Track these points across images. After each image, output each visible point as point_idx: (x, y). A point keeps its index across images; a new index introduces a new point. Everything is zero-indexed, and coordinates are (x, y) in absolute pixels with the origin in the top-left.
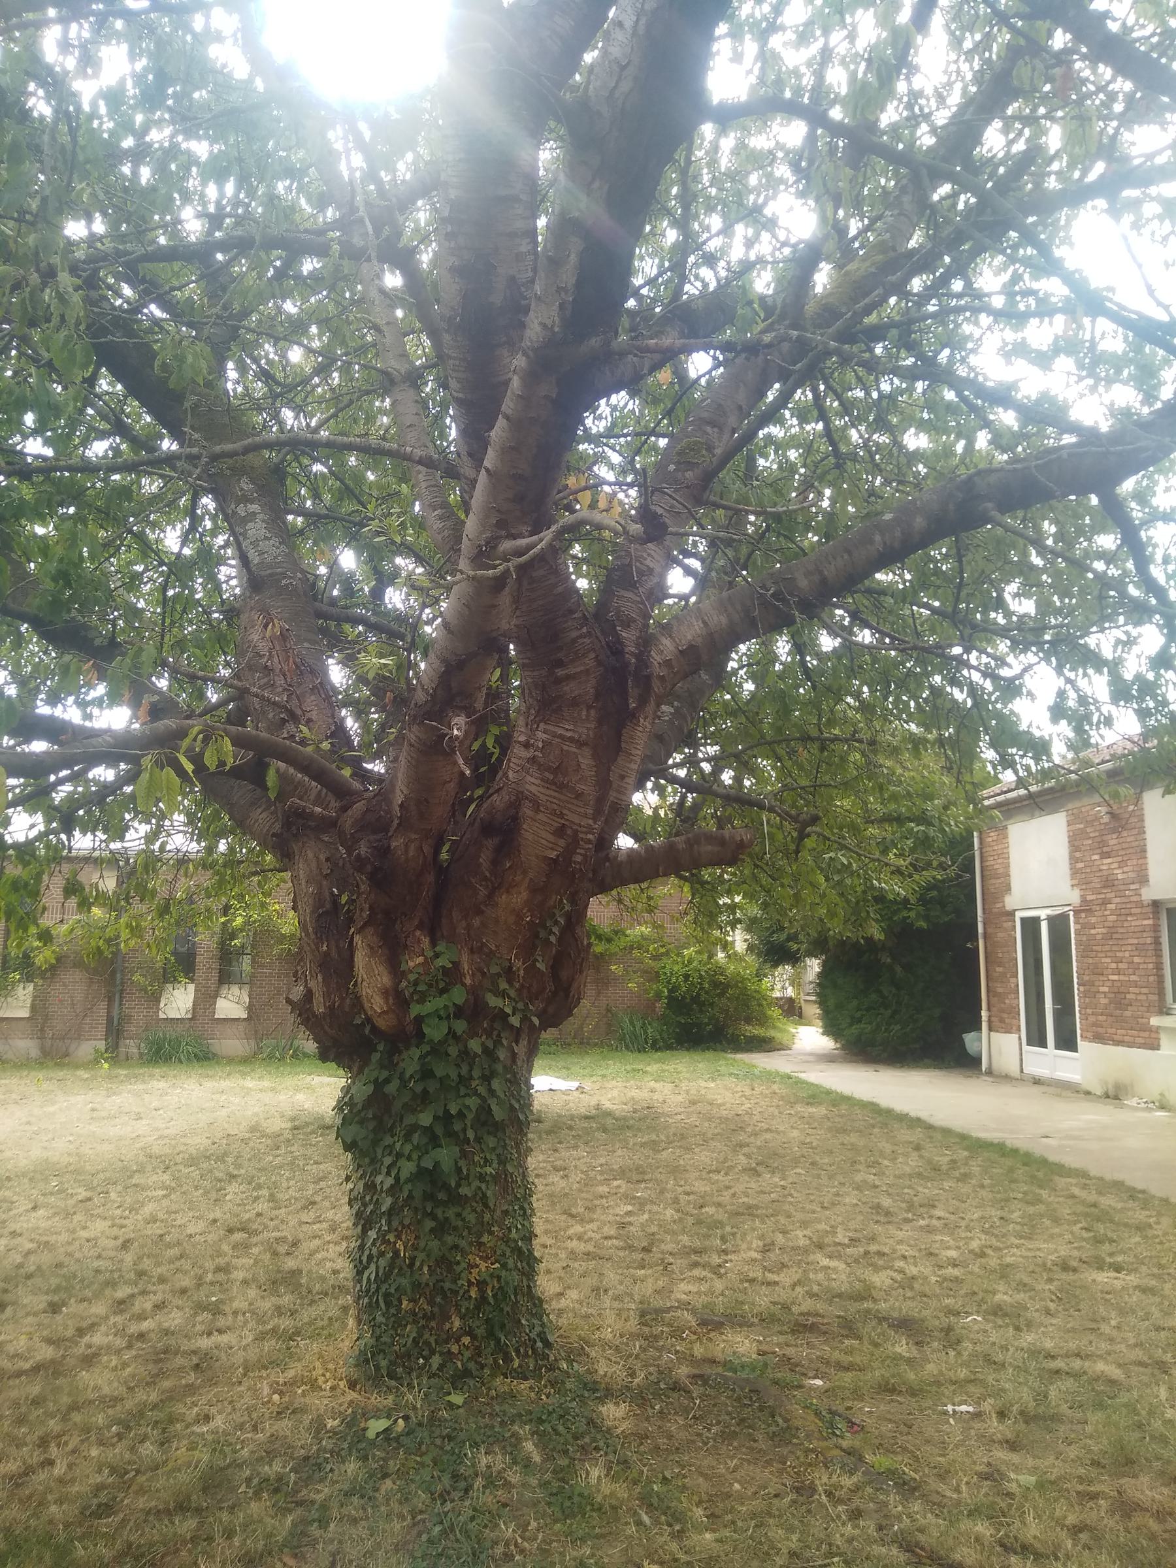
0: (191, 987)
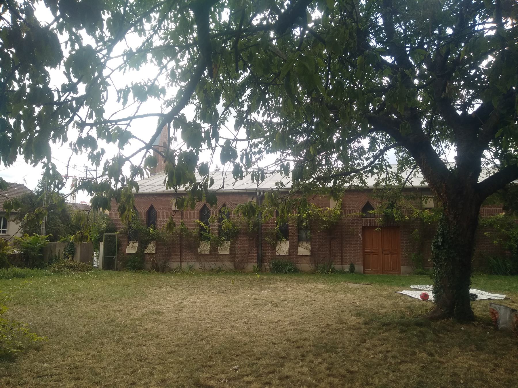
0: (288, 243)
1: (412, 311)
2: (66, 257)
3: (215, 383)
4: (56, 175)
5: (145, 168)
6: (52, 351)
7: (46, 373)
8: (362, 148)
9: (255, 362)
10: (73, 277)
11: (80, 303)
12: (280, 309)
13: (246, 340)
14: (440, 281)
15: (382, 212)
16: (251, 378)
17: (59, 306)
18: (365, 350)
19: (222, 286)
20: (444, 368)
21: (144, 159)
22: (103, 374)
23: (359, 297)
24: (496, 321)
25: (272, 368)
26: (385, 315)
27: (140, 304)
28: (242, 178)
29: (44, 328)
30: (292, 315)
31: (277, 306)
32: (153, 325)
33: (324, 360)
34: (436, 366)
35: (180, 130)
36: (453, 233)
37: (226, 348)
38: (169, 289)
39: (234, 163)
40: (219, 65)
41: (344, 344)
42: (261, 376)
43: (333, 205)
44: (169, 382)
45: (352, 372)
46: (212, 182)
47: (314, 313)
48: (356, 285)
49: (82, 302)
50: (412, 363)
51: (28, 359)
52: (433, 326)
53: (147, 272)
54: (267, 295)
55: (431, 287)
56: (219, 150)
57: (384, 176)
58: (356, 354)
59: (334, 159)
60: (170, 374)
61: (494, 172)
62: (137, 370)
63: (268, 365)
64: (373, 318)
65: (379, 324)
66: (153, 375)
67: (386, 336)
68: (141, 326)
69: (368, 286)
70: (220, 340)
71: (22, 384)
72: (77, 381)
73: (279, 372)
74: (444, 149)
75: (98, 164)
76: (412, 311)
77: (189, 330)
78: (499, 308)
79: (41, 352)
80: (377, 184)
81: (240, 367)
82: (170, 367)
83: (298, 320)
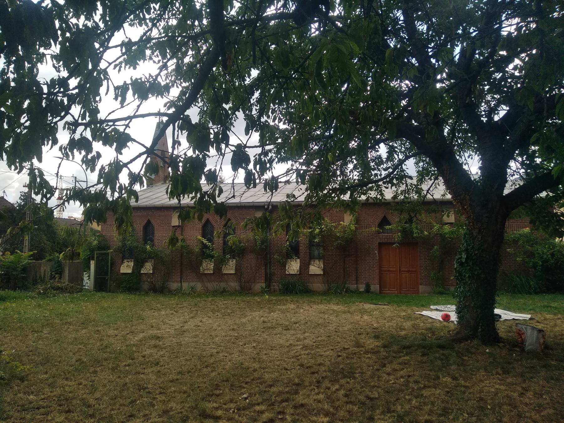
0: (298, 260)
1: (433, 333)
2: (53, 277)
3: (223, 413)
4: (44, 184)
5: (145, 175)
6: (39, 381)
7: (32, 405)
8: (380, 157)
9: (267, 389)
10: (61, 300)
11: (69, 328)
12: (292, 332)
13: (256, 365)
14: (464, 300)
15: (399, 228)
16: (263, 407)
17: (46, 332)
18: (385, 375)
19: (227, 308)
20: (470, 393)
21: (145, 165)
22: (97, 406)
23: (377, 318)
24: (523, 342)
25: (286, 396)
26: (405, 338)
27: (137, 329)
28: (255, 186)
29: (29, 356)
30: (305, 339)
31: (288, 329)
32: (152, 351)
33: (341, 386)
34: (461, 391)
35: (185, 133)
36: (480, 250)
37: (234, 375)
38: (169, 311)
39: (246, 169)
40: (222, 67)
41: (362, 369)
42: (274, 405)
43: (348, 219)
44: (171, 413)
45: (372, 399)
46: (221, 191)
47: (329, 336)
48: (372, 306)
49: (71, 327)
50: (435, 388)
51: (11, 390)
52: (457, 349)
53: (143, 293)
54: (277, 317)
55: (454, 307)
56: (229, 156)
57: (403, 187)
58: (376, 379)
59: (349, 169)
60: (173, 404)
61: (519, 184)
62: (135, 401)
63: (281, 393)
64: (392, 340)
65: (399, 347)
66: (153, 406)
67: (406, 360)
68: (139, 352)
69: (385, 307)
70: (227, 367)
71: (5, 419)
72: (68, 414)
73: (293, 400)
74: (467, 158)
75: (93, 170)
76: (433, 333)
77: (193, 356)
78: (526, 329)
79: (26, 383)
80: (395, 197)
81: (250, 395)
82: (172, 397)
83: (311, 343)
